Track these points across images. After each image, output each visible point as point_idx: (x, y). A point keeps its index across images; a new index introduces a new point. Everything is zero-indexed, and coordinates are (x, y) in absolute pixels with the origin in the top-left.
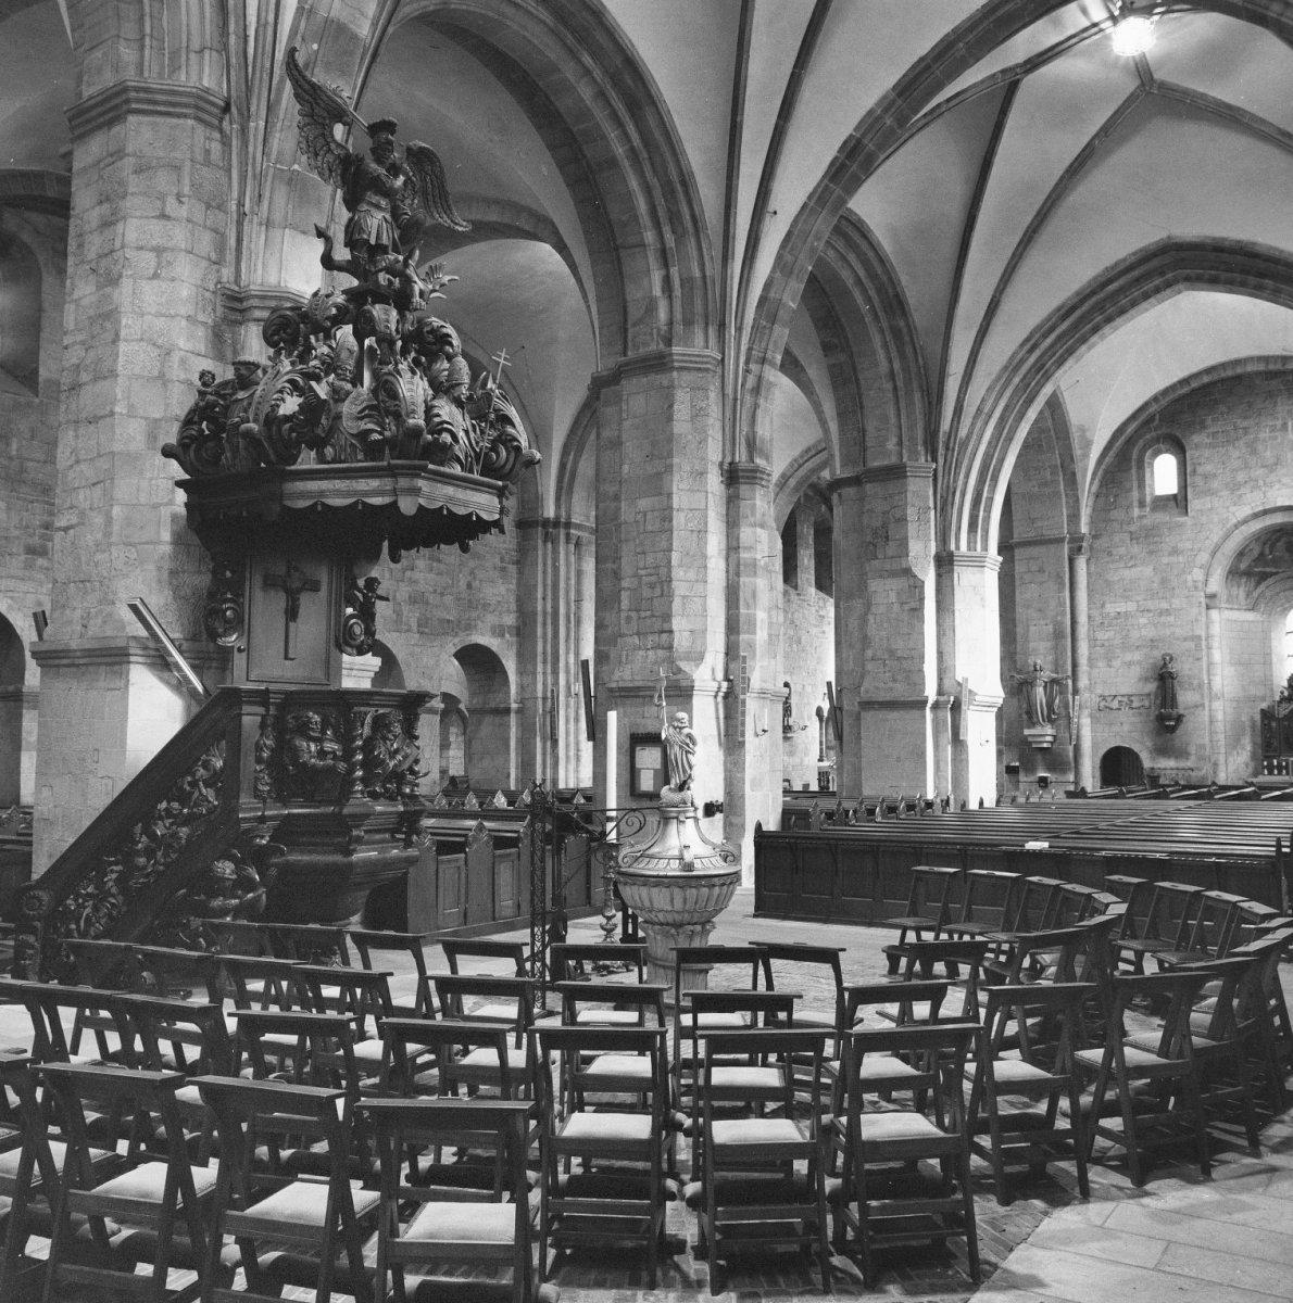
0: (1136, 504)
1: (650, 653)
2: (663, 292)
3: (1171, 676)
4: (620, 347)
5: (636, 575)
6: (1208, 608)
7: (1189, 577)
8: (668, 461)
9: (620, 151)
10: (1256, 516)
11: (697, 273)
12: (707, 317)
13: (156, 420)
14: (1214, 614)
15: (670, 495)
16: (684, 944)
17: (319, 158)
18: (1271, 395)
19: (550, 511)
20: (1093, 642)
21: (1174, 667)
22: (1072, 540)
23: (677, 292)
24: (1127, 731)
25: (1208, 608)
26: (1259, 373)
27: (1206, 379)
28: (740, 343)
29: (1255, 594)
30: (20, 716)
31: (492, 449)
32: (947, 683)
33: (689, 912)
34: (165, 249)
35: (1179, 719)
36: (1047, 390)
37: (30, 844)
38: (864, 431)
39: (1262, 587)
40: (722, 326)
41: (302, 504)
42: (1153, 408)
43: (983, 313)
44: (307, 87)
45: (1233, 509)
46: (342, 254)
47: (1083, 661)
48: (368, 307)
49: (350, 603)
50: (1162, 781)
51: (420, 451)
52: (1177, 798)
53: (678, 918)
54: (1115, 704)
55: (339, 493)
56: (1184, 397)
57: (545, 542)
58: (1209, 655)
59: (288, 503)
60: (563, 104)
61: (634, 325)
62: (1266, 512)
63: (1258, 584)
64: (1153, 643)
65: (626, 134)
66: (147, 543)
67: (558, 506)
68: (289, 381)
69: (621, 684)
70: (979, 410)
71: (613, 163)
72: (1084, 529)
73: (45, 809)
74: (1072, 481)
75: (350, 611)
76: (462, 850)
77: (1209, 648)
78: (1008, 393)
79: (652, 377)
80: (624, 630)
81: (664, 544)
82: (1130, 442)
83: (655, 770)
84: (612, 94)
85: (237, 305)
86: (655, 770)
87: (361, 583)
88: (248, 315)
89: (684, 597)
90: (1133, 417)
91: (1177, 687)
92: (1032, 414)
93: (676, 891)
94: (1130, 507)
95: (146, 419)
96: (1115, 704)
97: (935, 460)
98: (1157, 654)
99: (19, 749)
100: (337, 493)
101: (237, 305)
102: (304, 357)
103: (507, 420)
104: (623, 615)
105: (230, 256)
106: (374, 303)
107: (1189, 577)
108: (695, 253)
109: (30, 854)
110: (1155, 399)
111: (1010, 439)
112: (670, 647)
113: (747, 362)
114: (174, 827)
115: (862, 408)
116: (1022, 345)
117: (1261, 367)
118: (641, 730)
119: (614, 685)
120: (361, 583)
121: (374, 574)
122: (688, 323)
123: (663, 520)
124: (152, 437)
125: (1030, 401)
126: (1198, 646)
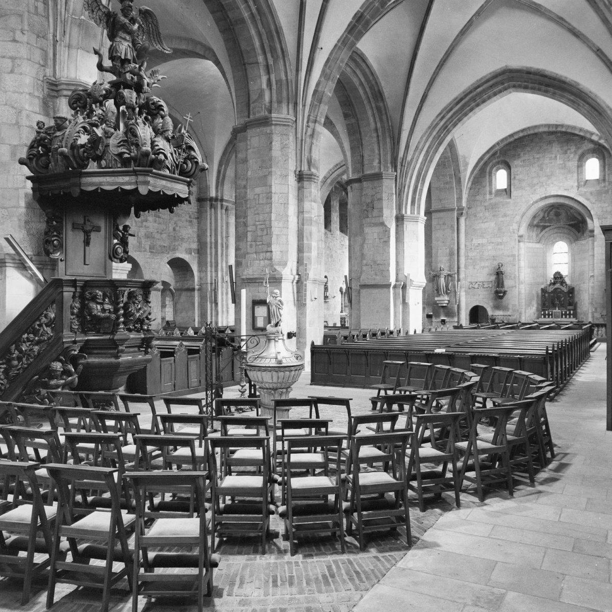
0: (488, 193)
1: (262, 262)
2: (267, 87)
4: (247, 114)
5: (254, 225)
7: (511, 227)
8: (270, 170)
9: (246, 15)
10: (542, 199)
11: (284, 78)
13: (15, 146)
14: (521, 244)
15: (270, 186)
16: (278, 398)
18: (550, 143)
19: (213, 194)
20: (467, 257)
21: (506, 269)
23: (274, 87)
24: (482, 299)
25: (519, 242)
26: (545, 132)
27: (521, 135)
29: (540, 235)
32: (400, 276)
33: (280, 383)
34: (16, 58)
35: (505, 293)
36: (448, 139)
38: (363, 157)
39: (544, 232)
40: (296, 104)
45: (531, 196)
46: (107, 63)
53: (275, 386)
54: (476, 286)
56: (510, 143)
57: (211, 208)
61: (253, 102)
63: (542, 231)
64: (494, 258)
67: (217, 191)
71: (243, 21)
72: (464, 204)
79: (262, 129)
80: (249, 250)
81: (268, 210)
83: (264, 317)
85: (55, 88)
86: (264, 317)
87: (121, 228)
88: (61, 93)
89: (277, 235)
92: (441, 149)
94: (485, 194)
96: (476, 286)
97: (396, 171)
98: (496, 263)
100: (108, 183)
101: (55, 88)
102: (89, 116)
105: (50, 63)
106: (124, 88)
107: (511, 227)
111: (431, 161)
112: (271, 259)
113: (308, 122)
117: (546, 129)
118: (257, 299)
119: (244, 277)
120: (121, 228)
122: (280, 102)
123: (268, 198)
124: (13, 154)
125: (440, 144)
126: (514, 259)
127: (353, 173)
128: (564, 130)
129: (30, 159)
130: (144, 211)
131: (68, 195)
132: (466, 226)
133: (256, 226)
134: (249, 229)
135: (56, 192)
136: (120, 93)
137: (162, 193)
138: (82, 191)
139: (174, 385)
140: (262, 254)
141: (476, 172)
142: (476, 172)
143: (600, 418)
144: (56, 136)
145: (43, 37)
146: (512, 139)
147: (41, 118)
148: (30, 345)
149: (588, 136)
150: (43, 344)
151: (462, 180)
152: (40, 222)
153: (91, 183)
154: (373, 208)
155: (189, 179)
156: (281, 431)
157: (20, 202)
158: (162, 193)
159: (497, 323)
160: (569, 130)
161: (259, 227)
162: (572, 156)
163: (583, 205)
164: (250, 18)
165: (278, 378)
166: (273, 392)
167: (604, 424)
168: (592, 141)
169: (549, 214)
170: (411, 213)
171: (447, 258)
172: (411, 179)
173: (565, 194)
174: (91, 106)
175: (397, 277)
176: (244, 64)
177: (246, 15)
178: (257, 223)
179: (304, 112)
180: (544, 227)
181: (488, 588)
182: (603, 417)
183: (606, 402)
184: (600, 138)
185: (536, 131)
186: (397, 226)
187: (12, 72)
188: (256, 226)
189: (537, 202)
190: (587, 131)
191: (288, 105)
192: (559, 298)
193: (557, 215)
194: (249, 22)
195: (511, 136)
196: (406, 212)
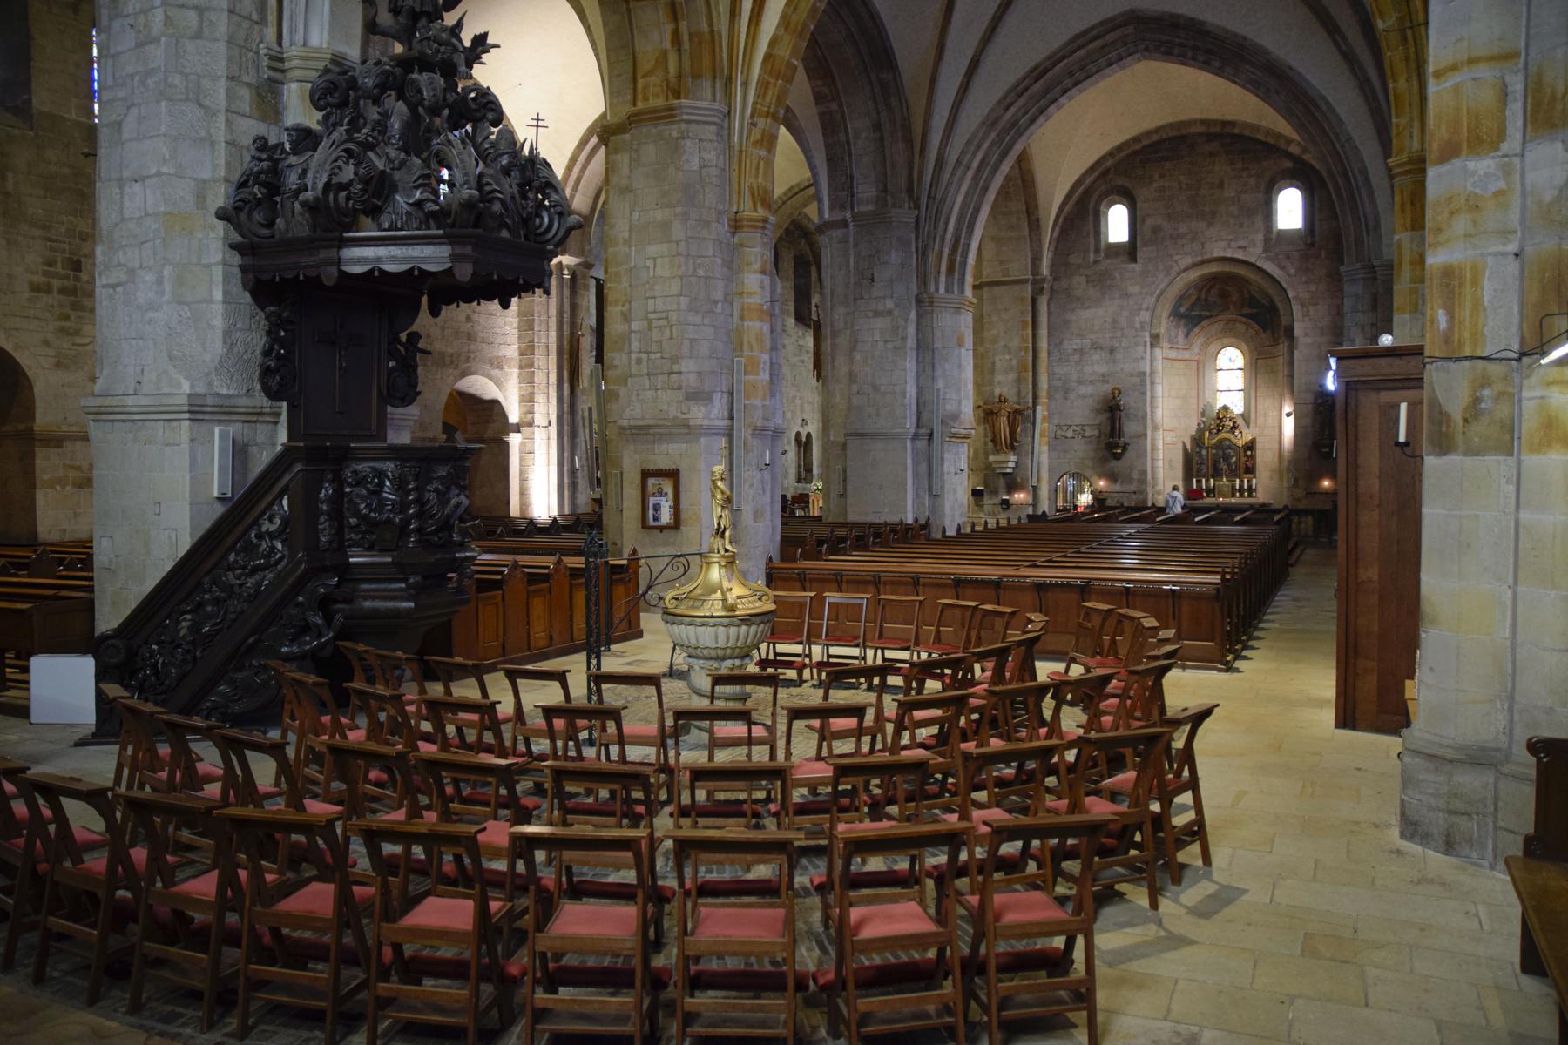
0: (1092, 249)
2: (672, 43)
3: (1118, 408)
4: (629, 97)
6: (1152, 346)
10: (1195, 265)
11: (706, 29)
12: (714, 71)
13: (204, 181)
14: (1158, 351)
20: (1051, 375)
21: (1123, 400)
22: (1035, 282)
23: (686, 45)
25: (1152, 346)
26: (1200, 134)
27: (1155, 138)
28: (745, 97)
30: (32, 455)
32: (925, 416)
34: (207, 9)
35: (1125, 448)
36: (1018, 147)
37: (91, 589)
38: (852, 177)
40: (729, 80)
41: (357, 269)
42: (1109, 163)
43: (963, 72)
47: (1043, 394)
48: (415, 76)
49: (391, 356)
50: (1109, 503)
52: (1125, 522)
53: (720, 652)
54: (1070, 433)
55: (394, 259)
56: (1135, 153)
58: (1152, 390)
59: (344, 268)
62: (1203, 262)
64: (1104, 379)
68: (346, 150)
69: (632, 422)
70: (959, 162)
72: (1045, 271)
73: (105, 559)
74: (1035, 225)
76: (500, 588)
77: (1153, 383)
78: (986, 145)
82: (1087, 193)
85: (279, 65)
87: (403, 336)
88: (289, 75)
89: (691, 340)
90: (1092, 169)
91: (1124, 418)
92: (1006, 167)
94: (1087, 251)
96: (1070, 433)
97: (917, 207)
98: (1106, 388)
99: (33, 486)
100: (393, 259)
101: (279, 65)
102: (354, 126)
104: (634, 356)
105: (272, 17)
106: (420, 72)
108: (704, 9)
109: (92, 602)
110: (1111, 154)
111: (985, 189)
115: (850, 155)
116: (999, 102)
118: (652, 466)
119: (625, 423)
120: (403, 336)
121: (414, 328)
122: (696, 76)
124: (201, 199)
125: (1004, 155)
126: (1143, 383)
127: (832, 208)
128: (1236, 131)
129: (237, 209)
130: (449, 303)
131: (315, 282)
132: (1049, 313)
134: (635, 326)
135: (290, 275)
136: (413, 81)
138: (343, 274)
140: (660, 378)
141: (1068, 208)
142: (1068, 208)
143: (1321, 703)
144: (290, 166)
146: (1138, 147)
147: (261, 129)
149: (1282, 145)
151: (1042, 223)
152: (250, 329)
153: (360, 258)
154: (872, 280)
156: (755, 749)
159: (1111, 508)
160: (1247, 133)
161: (655, 323)
162: (1252, 181)
163: (1274, 279)
167: (1329, 715)
168: (1289, 155)
169: (1208, 292)
170: (947, 291)
171: (1012, 376)
172: (947, 223)
173: (1240, 255)
174: (357, 105)
175: (918, 419)
178: (651, 316)
179: (745, 97)
180: (1201, 319)
181: (1168, 1024)
182: (1328, 701)
184: (1305, 150)
185: (1184, 132)
186: (919, 316)
187: (198, 35)
188: (650, 322)
189: (1186, 270)
190: (1279, 136)
191: (714, 87)
192: (1227, 458)
193: (1224, 295)
195: (1136, 139)
196: (937, 290)
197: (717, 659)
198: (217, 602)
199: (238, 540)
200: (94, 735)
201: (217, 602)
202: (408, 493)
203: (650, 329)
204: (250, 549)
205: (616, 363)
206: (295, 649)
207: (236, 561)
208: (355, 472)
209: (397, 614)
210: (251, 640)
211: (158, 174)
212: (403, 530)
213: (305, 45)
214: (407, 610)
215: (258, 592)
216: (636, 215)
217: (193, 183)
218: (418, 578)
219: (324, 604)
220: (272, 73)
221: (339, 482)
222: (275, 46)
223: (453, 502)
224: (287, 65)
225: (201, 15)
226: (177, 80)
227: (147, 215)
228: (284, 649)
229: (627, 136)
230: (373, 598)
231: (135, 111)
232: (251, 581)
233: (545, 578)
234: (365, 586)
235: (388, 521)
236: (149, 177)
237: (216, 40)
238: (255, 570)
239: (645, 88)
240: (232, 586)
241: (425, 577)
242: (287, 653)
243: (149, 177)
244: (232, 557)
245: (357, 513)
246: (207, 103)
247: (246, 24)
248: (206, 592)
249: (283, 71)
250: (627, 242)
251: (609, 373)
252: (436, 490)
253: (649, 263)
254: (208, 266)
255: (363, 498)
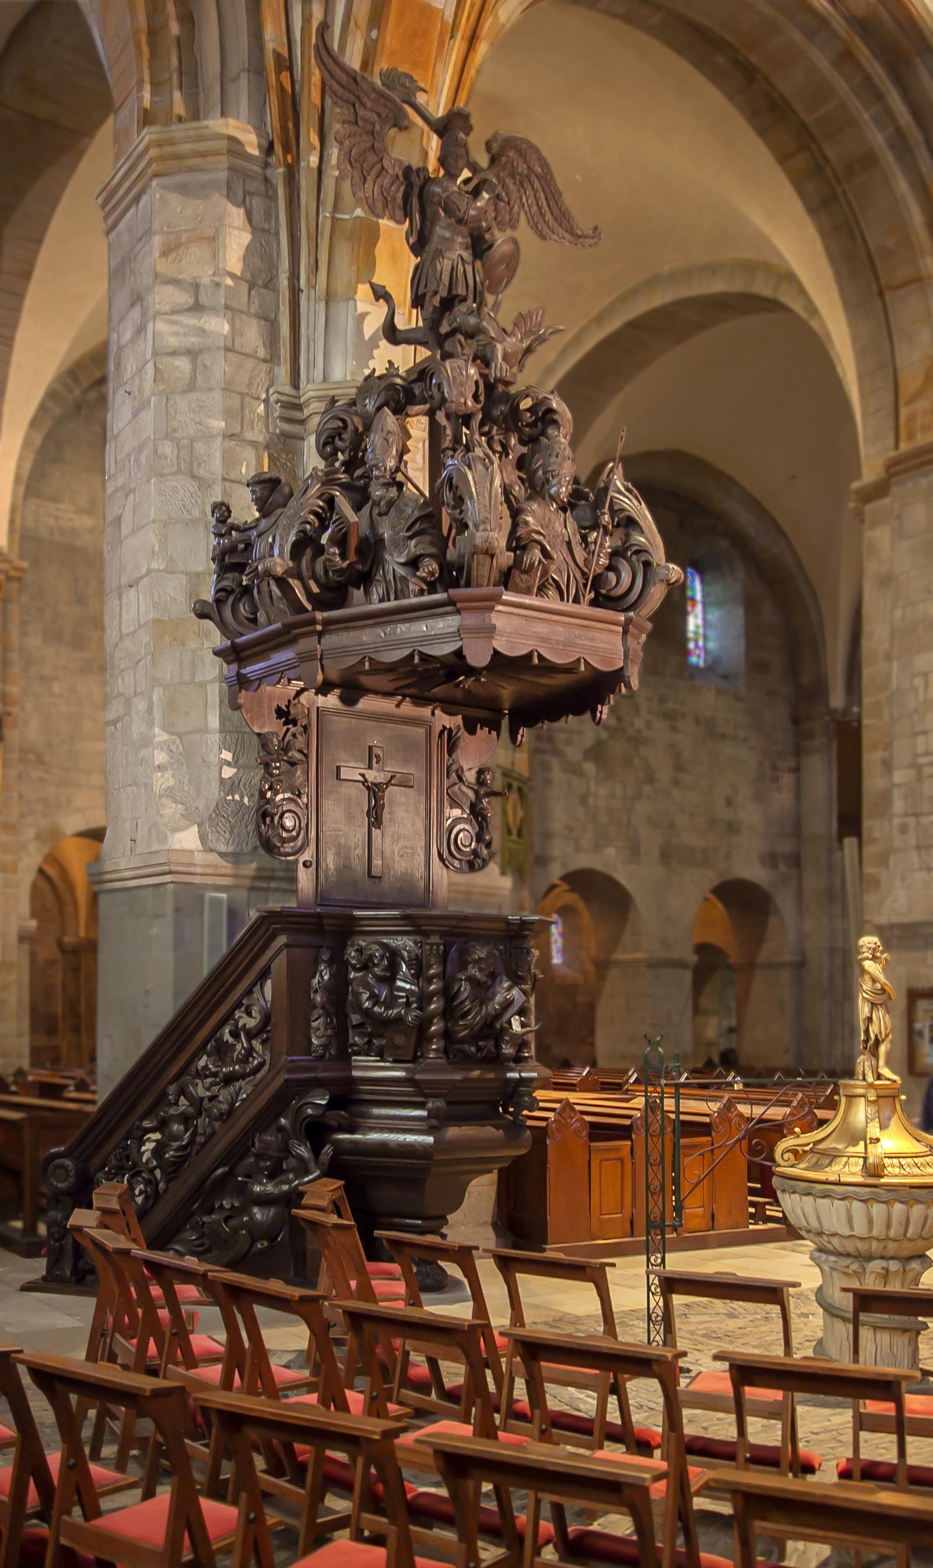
4: (891, 440)
9: (878, 139)
13: (198, 575)
16: (871, 1284)
17: (369, 184)
31: (610, 568)
33: (878, 1240)
34: (201, 351)
44: (344, 78)
46: (407, 319)
49: (455, 804)
51: (495, 575)
53: (862, 1247)
60: (789, 85)
61: (910, 402)
65: (888, 110)
66: (193, 732)
71: (869, 160)
75: (457, 812)
80: (897, 843)
84: (864, 53)
85: (297, 415)
93: (856, 1205)
95: (187, 574)
103: (630, 523)
104: (896, 821)
105: (285, 352)
114: (215, 1089)
133: (919, 768)
134: (898, 777)
137: (536, 661)
139: (632, 1223)
145: (266, 286)
148: (212, 1084)
150: (242, 1083)
155: (622, 618)
157: (210, 718)
158: (536, 661)
164: (891, 147)
165: (870, 1222)
166: (855, 1266)
176: (881, 294)
177: (878, 139)
178: (922, 760)
183: (211, 1536)
187: (191, 387)
194: (889, 158)
197: (857, 1256)
198: (186, 1119)
199: (208, 1041)
200: (44, 1278)
201: (186, 1119)
202: (430, 981)
203: (920, 779)
204: (222, 1051)
205: (876, 834)
206: (270, 1188)
207: (206, 1067)
208: (360, 951)
209: (409, 1151)
210: (220, 1171)
211: (149, 572)
212: (422, 1035)
213: (325, 379)
214: (426, 1147)
215: (231, 1111)
216: (898, 613)
217: (184, 579)
218: (440, 1103)
219: (316, 1132)
220: (287, 427)
221: (339, 966)
222: (288, 389)
223: (499, 998)
224: (306, 412)
225: (194, 362)
226: (168, 449)
227: (140, 626)
228: (257, 1188)
229: (886, 501)
230: (381, 1130)
231: (131, 497)
232: (224, 1095)
233: (704, 1129)
234: (377, 1111)
235: (399, 1020)
236: (142, 578)
237: (211, 389)
238: (229, 1080)
239: (911, 419)
240: (202, 1099)
241: (449, 1103)
242: (259, 1194)
243: (142, 578)
244: (202, 1063)
245: (358, 1007)
246: (201, 472)
247: (250, 363)
248: (171, 1105)
249: (302, 422)
250: (888, 657)
251: (867, 850)
252: (471, 980)
253: (918, 682)
254: (203, 685)
255: (367, 986)
